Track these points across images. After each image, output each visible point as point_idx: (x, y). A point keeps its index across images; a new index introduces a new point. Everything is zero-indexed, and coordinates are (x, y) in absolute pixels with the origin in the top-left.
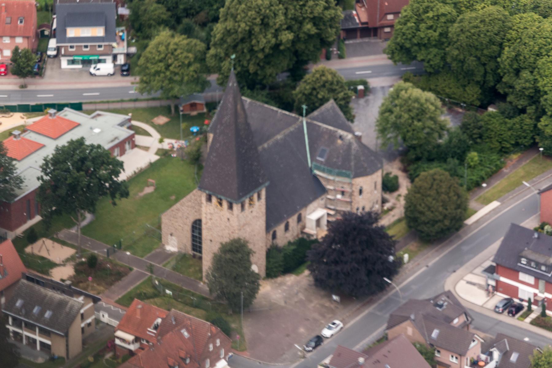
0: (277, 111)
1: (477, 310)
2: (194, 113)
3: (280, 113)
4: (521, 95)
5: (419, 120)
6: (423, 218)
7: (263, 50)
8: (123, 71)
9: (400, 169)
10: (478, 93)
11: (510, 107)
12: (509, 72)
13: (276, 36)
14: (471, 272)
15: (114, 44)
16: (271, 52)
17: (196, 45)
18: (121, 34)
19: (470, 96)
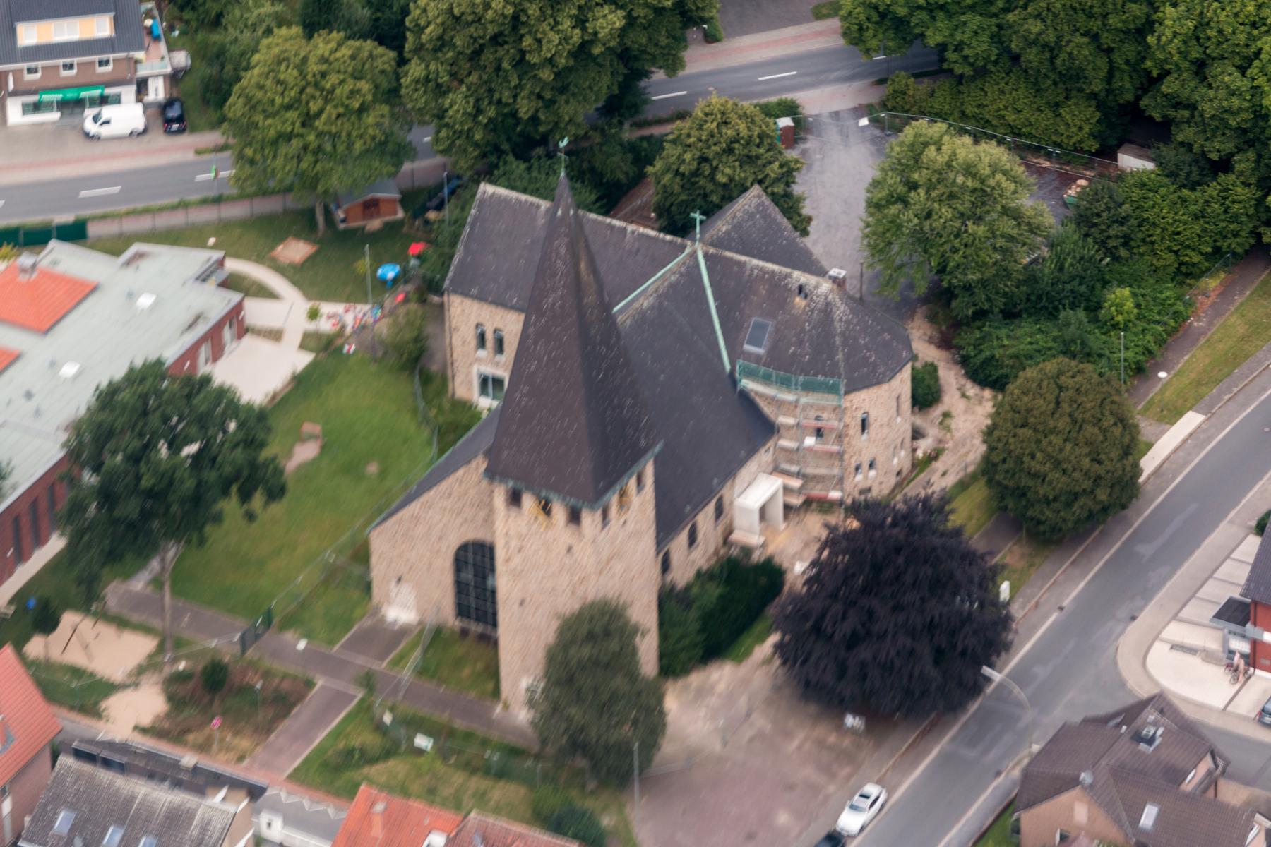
0: (625, 229)
1: (1214, 721)
2: (375, 224)
3: (633, 232)
4: (1219, 124)
5: (979, 219)
6: (1042, 490)
7: (551, 61)
8: (169, 122)
9: (930, 341)
10: (1093, 121)
11: (1188, 158)
12: (1179, 69)
13: (580, 22)
14: (1175, 617)
15: (140, 55)
16: (571, 62)
17: (371, 56)
18: (148, 22)
19: (1074, 129)
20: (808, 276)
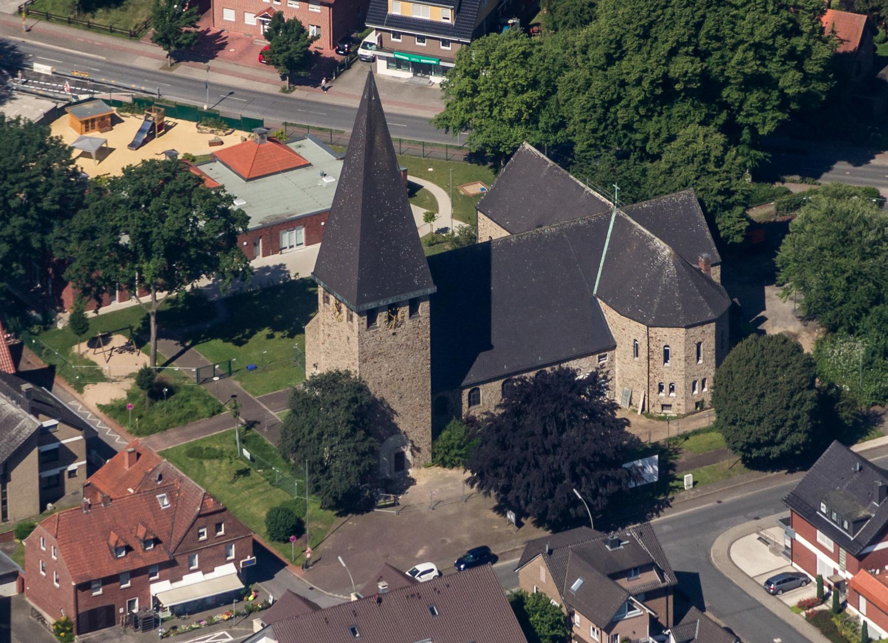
0: (584, 189)
20: (662, 243)
